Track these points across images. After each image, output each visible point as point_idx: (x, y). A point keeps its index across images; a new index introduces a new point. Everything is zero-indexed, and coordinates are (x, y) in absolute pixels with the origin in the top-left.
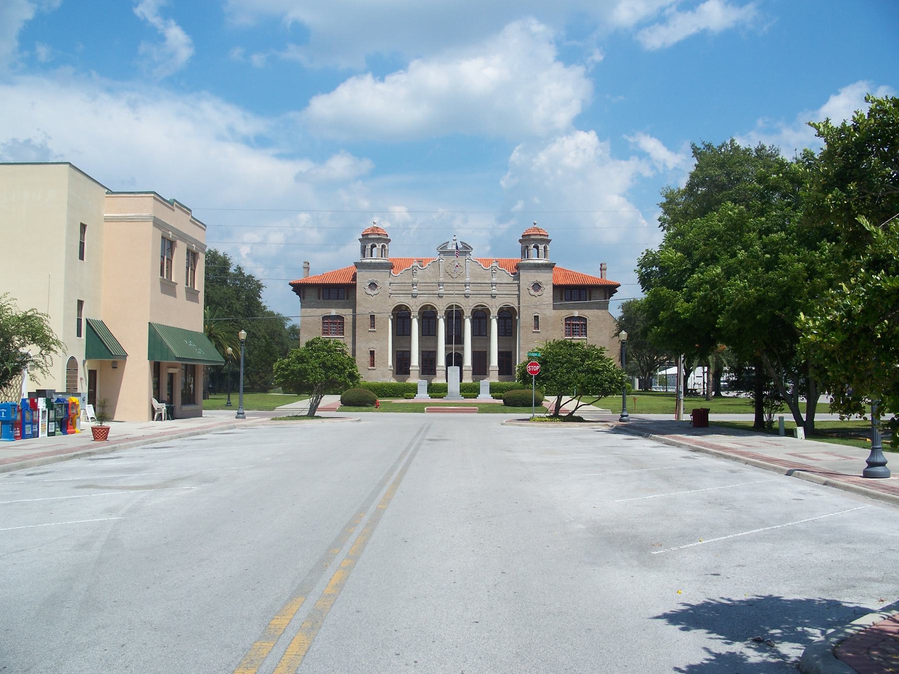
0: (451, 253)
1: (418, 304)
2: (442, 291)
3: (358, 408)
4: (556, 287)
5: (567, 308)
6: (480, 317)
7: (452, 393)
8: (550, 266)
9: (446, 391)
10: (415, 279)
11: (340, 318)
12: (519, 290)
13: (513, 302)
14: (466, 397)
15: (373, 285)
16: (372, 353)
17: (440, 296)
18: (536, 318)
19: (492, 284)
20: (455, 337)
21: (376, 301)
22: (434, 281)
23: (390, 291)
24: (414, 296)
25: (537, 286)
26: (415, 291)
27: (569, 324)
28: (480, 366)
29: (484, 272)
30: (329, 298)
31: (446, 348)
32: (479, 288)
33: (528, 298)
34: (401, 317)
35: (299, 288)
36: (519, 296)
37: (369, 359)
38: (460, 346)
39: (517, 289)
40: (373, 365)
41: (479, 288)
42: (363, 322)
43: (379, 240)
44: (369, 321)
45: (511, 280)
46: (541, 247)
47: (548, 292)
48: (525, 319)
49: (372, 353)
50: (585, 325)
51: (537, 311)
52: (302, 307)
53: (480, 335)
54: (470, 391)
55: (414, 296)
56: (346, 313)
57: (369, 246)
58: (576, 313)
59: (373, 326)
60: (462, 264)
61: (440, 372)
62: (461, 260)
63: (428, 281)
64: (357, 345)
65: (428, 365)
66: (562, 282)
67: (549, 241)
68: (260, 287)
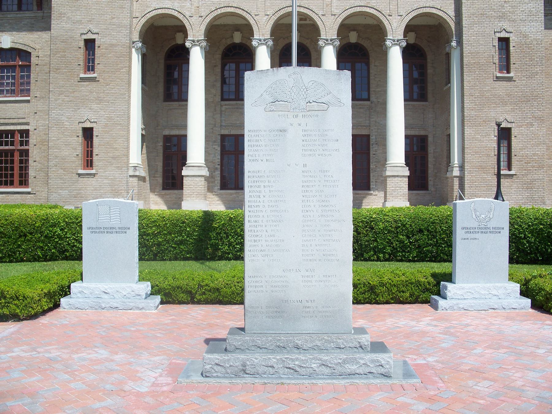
11: (22, 54)
16: (88, 133)
18: (504, 42)
34: (164, 48)
40: (89, 163)
48: (476, 45)
49: (88, 133)
51: (506, 25)
59: (90, 66)
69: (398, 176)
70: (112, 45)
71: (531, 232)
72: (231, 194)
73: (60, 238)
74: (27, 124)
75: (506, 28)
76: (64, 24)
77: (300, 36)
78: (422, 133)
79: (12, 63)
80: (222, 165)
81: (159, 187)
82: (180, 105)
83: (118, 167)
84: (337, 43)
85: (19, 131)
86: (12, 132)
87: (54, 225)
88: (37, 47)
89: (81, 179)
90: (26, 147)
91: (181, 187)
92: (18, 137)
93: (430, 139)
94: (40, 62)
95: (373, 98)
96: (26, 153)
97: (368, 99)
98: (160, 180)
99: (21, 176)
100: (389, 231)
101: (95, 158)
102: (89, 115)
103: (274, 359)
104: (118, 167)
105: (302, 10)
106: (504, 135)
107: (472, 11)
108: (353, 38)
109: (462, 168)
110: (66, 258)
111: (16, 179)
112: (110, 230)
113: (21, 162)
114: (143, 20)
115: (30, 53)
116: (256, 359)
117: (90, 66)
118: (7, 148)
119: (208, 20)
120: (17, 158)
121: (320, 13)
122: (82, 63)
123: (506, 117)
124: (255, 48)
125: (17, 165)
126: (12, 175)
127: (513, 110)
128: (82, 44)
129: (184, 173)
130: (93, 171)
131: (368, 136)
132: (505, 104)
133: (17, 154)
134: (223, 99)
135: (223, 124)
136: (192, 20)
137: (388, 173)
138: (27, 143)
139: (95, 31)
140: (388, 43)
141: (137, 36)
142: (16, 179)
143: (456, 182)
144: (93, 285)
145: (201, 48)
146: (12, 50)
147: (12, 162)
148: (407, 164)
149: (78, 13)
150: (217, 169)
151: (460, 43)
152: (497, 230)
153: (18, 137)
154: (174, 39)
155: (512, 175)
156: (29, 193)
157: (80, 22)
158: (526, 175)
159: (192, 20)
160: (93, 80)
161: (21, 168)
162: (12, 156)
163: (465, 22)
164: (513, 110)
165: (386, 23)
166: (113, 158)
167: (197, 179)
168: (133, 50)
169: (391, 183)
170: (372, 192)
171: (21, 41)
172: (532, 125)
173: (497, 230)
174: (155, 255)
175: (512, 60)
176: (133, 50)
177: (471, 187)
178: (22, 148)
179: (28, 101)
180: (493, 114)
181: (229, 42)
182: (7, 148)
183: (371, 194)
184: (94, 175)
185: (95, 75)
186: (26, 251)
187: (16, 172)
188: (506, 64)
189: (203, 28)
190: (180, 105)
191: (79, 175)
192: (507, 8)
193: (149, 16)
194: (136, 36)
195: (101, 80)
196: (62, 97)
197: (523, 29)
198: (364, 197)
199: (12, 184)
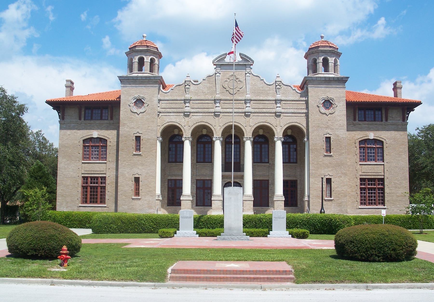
0: (229, 66)
1: (191, 124)
2: (218, 109)
3: (145, 235)
4: (350, 105)
5: (361, 129)
6: (263, 139)
7: (230, 229)
8: (342, 81)
9: (222, 226)
10: (188, 96)
11: (103, 141)
12: (307, 108)
13: (300, 122)
14: (252, 235)
15: (139, 102)
16: (137, 180)
17: (216, 115)
18: (328, 139)
19: (276, 101)
20: (232, 165)
21: (142, 122)
22: (210, 98)
23: (159, 109)
24: (187, 115)
25: (328, 103)
26: (187, 109)
27: (364, 148)
28: (262, 194)
29: (266, 88)
30: (92, 119)
31: (223, 176)
32: (261, 106)
33: (319, 116)
34: (171, 139)
35: (56, 105)
36: (307, 115)
37: (133, 187)
38: (239, 173)
39: (304, 106)
40: (137, 193)
41: (261, 106)
42: (128, 144)
43: (147, 52)
44: (134, 143)
45: (297, 97)
46: (331, 60)
47: (340, 111)
48: (314, 141)
49: (137, 180)
50: (382, 148)
51: (329, 131)
52: (61, 128)
53: (261, 162)
54: (257, 226)
55: (187, 115)
56: (109, 135)
57: (136, 60)
58: (371, 135)
59: (138, 148)
60: (242, 78)
61: (216, 203)
62: (240, 74)
63: (202, 97)
64: (120, 170)
65: (203, 193)
66: (353, 99)
67: (338, 55)
68: (22, 109)
70: (148, 139)
71: (319, 223)
72: (201, 208)
73: (143, 224)
74: (105, 174)
75: (329, 132)
76: (126, 129)
77: (235, 132)
78: (294, 179)
79: (97, 144)
80: (196, 194)
81: (166, 205)
83: (151, 196)
84: (252, 139)
85: (91, 178)
86: (97, 178)
87: (141, 220)
88: (110, 137)
89: (133, 201)
90: (104, 185)
91: (180, 205)
92: (100, 180)
93: (298, 182)
94: (111, 145)
95: (270, 162)
96: (104, 188)
97: (268, 163)
98: (166, 201)
99: (101, 198)
100: (267, 223)
101: (140, 191)
103: (229, 237)
104: (151, 196)
105: (236, 124)
107: (314, 125)
108: (261, 132)
109: (309, 196)
110: (145, 232)
111: (99, 200)
112: (187, 217)
113: (101, 192)
114: (162, 127)
116: (226, 237)
117: (138, 148)
118: (94, 185)
119: (193, 128)
120: (99, 190)
121: (244, 125)
122: (134, 147)
123: (327, 173)
124: (214, 142)
125: (99, 193)
126: (97, 198)
127: (332, 170)
128: (134, 138)
129: (181, 199)
130: (140, 197)
131: (268, 180)
133: (99, 188)
134: (197, 162)
135: (197, 174)
136: (185, 128)
137: (275, 199)
138: (105, 183)
140: (275, 139)
141: (160, 135)
142: (99, 200)
143: (306, 203)
144: (182, 231)
145: (189, 141)
147: (97, 192)
148: (284, 194)
149: (132, 124)
150: (194, 196)
151: (308, 139)
152: (283, 218)
153: (100, 180)
154: (173, 132)
155: (332, 200)
156: (105, 207)
157: (133, 128)
158: (338, 200)
159: (185, 128)
160: (140, 155)
161: (101, 195)
162: (97, 189)
163: (310, 130)
165: (274, 130)
167: (188, 201)
168: (158, 141)
169: (276, 204)
171: (102, 134)
172: (341, 177)
173: (283, 218)
175: (332, 148)
176: (158, 141)
177: (312, 205)
178: (102, 185)
179: (106, 163)
180: (323, 172)
181: (200, 134)
182: (94, 185)
184: (140, 199)
185: (140, 153)
186: (131, 230)
187: (99, 196)
188: (329, 149)
189: (190, 131)
191: (133, 199)
192: (330, 123)
193: (165, 125)
194: (159, 135)
195: (143, 155)
197: (337, 133)
198: (267, 210)
199: (96, 202)
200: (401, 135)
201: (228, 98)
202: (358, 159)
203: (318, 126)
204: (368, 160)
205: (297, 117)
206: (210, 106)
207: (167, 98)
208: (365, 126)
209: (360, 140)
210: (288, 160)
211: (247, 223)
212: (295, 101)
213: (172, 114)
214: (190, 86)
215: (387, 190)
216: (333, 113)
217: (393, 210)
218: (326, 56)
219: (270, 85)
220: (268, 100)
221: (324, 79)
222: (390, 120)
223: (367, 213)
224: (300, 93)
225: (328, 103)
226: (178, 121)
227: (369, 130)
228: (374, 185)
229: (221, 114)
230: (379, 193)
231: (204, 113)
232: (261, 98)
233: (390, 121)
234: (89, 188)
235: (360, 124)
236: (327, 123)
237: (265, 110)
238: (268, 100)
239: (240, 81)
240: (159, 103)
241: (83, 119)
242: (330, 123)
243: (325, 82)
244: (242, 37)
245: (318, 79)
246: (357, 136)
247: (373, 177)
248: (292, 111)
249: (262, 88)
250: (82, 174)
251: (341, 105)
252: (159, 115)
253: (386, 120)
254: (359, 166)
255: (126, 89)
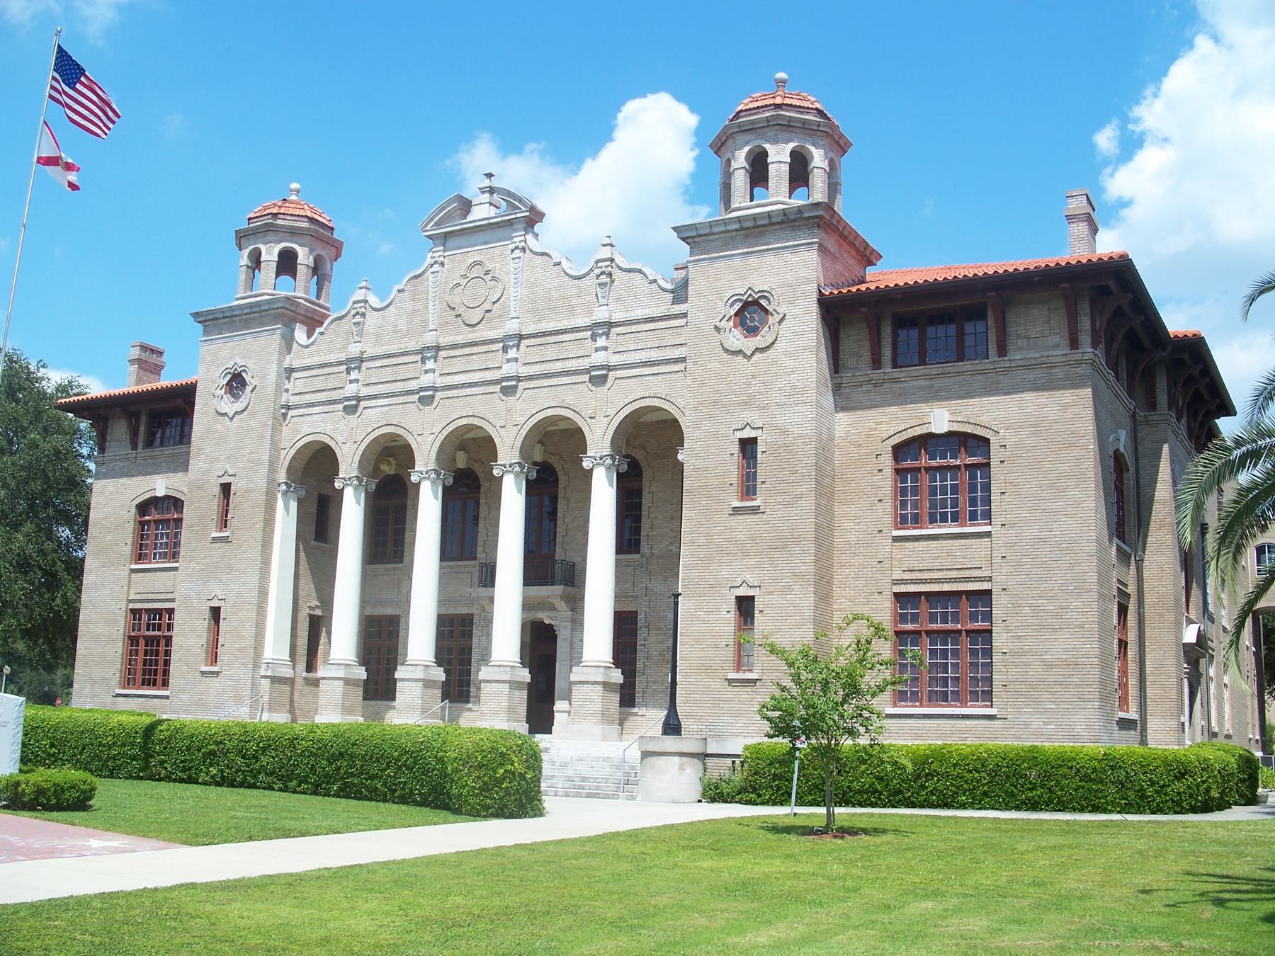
5: (902, 399)
32: (550, 353)
41: (550, 353)
47: (799, 332)
48: (705, 458)
51: (751, 416)
69: (587, 682)
75: (750, 421)
79: (168, 516)
82: (386, 570)
83: (243, 664)
85: (148, 611)
93: (641, 617)
102: (219, 590)
106: (745, 606)
111: (159, 682)
115: (986, 441)
125: (161, 663)
127: (759, 565)
132: (745, 553)
139: (231, 471)
142: (159, 682)
146: (950, 434)
164: (759, 565)
166: (240, 650)
167: (336, 683)
170: (636, 710)
172: (789, 589)
174: (111, 772)
178: (148, 633)
183: (636, 714)
190: (386, 570)
191: (203, 673)
192: (757, 385)
196: (193, 564)
200: (1065, 407)
201: (459, 339)
202: (888, 519)
203: (716, 402)
204: (933, 520)
205: (660, 377)
206: (411, 371)
207: (307, 362)
208: (917, 383)
209: (897, 440)
210: (629, 538)
211: (33, 728)
212: (653, 320)
213: (316, 410)
214: (363, 315)
215: (1000, 640)
216: (768, 347)
217: (1027, 725)
218: (757, 143)
219: (579, 278)
220: (572, 330)
221: (737, 226)
222: (1021, 349)
223: (917, 737)
224: (672, 291)
225: (751, 312)
226: (329, 428)
227: (934, 396)
228: (956, 618)
229: (439, 395)
230: (974, 653)
231: (394, 395)
232: (552, 326)
233: (1015, 355)
234: (142, 642)
235: (896, 381)
236: (748, 384)
237: (559, 366)
238: (572, 330)
239: (494, 279)
240: (288, 378)
241: (140, 445)
242: (757, 385)
243: (746, 237)
244: (119, 117)
245: (715, 230)
246: (884, 427)
247: (946, 587)
248: (643, 356)
249: (557, 289)
250: (131, 601)
251: (798, 311)
252: (285, 416)
253: (1002, 351)
254: (887, 546)
255: (211, 347)
